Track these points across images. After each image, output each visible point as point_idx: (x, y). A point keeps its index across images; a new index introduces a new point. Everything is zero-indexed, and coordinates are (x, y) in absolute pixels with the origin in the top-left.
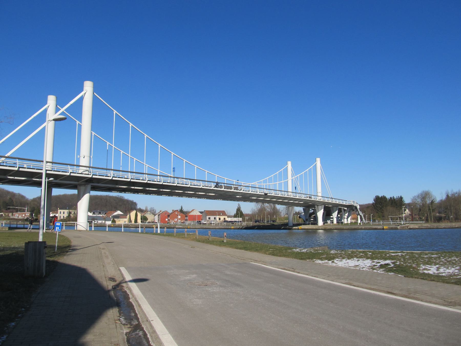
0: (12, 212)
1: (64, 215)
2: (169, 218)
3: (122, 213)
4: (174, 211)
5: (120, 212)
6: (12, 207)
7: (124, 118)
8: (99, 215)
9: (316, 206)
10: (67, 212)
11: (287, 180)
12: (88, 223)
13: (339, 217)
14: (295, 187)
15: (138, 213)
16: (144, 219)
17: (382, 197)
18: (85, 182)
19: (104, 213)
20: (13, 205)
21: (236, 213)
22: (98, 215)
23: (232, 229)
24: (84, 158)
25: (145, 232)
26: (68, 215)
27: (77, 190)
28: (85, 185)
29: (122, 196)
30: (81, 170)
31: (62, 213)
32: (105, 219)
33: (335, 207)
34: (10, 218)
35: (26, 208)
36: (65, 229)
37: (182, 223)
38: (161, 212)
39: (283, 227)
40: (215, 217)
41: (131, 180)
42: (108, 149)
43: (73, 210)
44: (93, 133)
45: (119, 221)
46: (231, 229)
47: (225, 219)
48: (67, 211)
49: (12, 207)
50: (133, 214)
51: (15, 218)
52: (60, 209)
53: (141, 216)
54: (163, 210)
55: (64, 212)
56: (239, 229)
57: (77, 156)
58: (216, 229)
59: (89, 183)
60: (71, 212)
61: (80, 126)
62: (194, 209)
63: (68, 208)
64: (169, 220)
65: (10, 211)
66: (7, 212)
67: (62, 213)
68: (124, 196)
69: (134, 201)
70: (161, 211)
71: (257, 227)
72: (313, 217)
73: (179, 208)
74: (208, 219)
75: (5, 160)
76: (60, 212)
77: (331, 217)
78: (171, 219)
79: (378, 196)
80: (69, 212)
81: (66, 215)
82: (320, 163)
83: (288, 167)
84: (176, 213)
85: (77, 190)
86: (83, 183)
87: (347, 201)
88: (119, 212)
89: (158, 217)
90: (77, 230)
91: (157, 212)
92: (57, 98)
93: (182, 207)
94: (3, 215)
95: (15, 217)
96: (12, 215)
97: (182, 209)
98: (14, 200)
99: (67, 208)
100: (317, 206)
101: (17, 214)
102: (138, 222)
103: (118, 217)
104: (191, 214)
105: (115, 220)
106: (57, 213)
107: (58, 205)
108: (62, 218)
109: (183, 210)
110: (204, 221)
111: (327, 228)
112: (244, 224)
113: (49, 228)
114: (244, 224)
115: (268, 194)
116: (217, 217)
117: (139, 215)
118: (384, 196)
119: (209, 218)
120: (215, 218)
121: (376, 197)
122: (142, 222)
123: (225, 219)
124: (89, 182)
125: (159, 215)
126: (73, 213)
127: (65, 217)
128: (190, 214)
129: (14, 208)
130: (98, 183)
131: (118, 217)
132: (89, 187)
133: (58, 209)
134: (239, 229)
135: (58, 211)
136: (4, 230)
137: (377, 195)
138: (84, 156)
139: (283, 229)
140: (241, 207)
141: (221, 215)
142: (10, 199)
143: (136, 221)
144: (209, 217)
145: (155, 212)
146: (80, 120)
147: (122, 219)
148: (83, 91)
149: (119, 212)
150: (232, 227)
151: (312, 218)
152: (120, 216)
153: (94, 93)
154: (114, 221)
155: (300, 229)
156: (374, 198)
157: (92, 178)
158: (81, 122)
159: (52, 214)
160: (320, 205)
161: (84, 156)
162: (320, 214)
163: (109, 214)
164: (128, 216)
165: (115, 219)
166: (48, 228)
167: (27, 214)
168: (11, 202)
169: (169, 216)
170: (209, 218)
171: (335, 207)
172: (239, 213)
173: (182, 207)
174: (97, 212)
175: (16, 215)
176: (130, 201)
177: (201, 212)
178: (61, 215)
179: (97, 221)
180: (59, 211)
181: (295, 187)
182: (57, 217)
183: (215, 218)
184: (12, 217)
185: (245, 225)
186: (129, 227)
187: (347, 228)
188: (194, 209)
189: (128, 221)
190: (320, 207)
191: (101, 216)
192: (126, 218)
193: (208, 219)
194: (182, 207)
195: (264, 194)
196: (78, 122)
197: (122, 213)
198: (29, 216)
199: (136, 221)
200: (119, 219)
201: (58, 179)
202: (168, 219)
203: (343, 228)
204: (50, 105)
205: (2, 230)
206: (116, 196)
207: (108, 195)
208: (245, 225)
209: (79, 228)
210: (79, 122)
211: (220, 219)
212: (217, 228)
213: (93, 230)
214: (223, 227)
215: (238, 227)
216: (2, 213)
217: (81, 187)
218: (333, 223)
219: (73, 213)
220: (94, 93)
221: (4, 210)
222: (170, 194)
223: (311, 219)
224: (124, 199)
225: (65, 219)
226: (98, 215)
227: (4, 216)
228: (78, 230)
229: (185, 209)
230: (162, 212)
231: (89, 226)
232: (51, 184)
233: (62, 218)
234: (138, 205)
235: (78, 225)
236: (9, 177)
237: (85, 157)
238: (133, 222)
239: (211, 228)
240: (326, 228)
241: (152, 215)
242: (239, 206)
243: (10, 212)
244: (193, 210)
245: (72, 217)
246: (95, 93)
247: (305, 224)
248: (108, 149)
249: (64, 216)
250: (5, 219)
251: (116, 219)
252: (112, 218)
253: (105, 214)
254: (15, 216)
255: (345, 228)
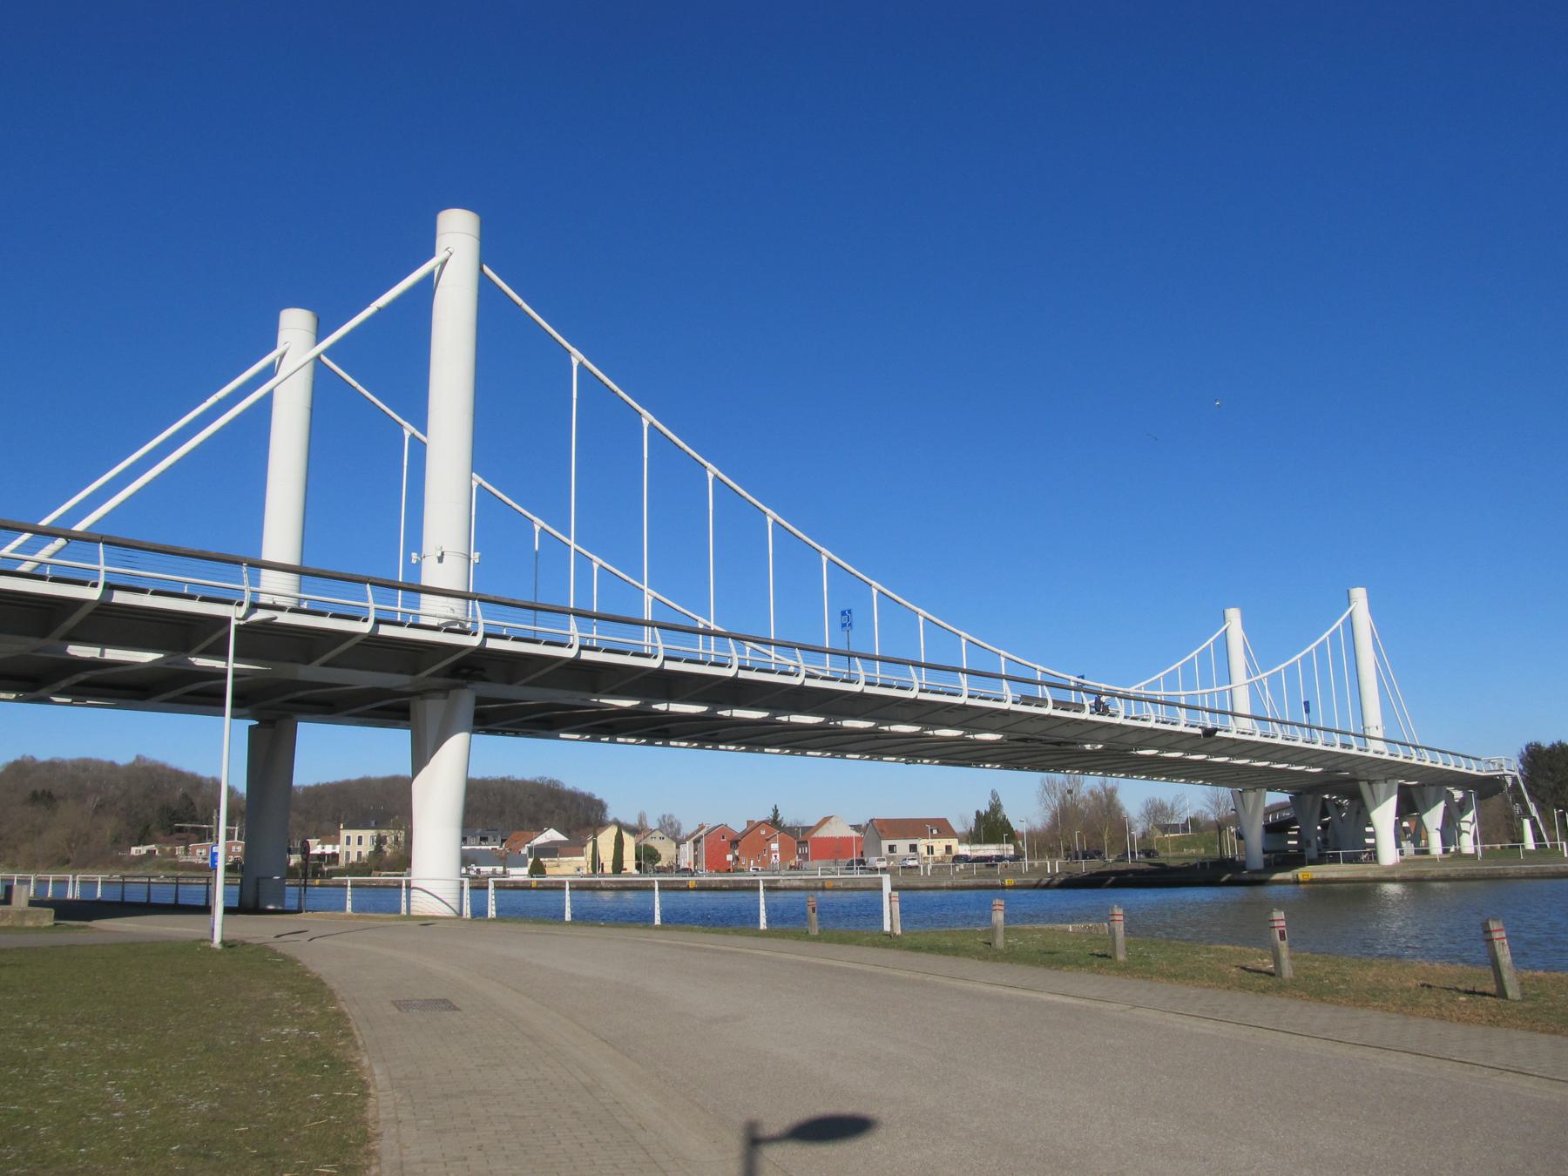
0: (184, 841)
1: (359, 848)
2: (737, 853)
3: (561, 837)
4: (753, 827)
5: (555, 832)
6: (190, 825)
7: (615, 388)
8: (480, 844)
9: (1364, 786)
10: (372, 837)
11: (1229, 687)
12: (462, 882)
13: (1404, 829)
14: (1307, 704)
15: (625, 835)
16: (647, 857)
17: (1553, 746)
18: (446, 676)
19: (499, 838)
20: (193, 819)
21: (973, 826)
22: (478, 847)
23: (1010, 887)
24: (440, 559)
25: (816, 933)
26: (373, 850)
27: (410, 731)
28: (445, 691)
29: (555, 779)
30: (434, 609)
31: (354, 840)
32: (505, 860)
33: (1432, 785)
34: (177, 863)
35: (237, 828)
36: (353, 909)
37: (791, 867)
38: (705, 830)
39: (1229, 875)
40: (913, 842)
41: (663, 663)
42: (537, 548)
43: (393, 831)
44: (477, 479)
45: (558, 866)
46: (1003, 887)
47: (948, 848)
48: (372, 833)
49: (190, 825)
50: (606, 840)
51: (193, 863)
52: (346, 827)
53: (638, 847)
54: (711, 822)
55: (360, 839)
56: (1036, 887)
57: (407, 558)
58: (942, 888)
59: (465, 681)
60: (386, 837)
61: (419, 449)
62: (832, 817)
63: (373, 823)
64: (737, 859)
65: (177, 839)
66: (167, 843)
67: (354, 840)
68: (561, 780)
69: (598, 797)
70: (702, 827)
71: (1113, 878)
72: (1296, 833)
73: (767, 814)
74: (885, 850)
75: (51, 557)
76: (348, 838)
77: (1368, 829)
78: (743, 856)
79: (1538, 746)
80: (379, 835)
81: (367, 848)
82: (1370, 611)
83: (1228, 630)
84: (763, 833)
85: (410, 731)
86: (440, 681)
87: (1479, 760)
88: (552, 835)
89: (695, 850)
90: (409, 917)
91: (687, 829)
92: (318, 320)
93: (776, 811)
94: (157, 852)
95: (195, 860)
96: (186, 850)
97: (779, 819)
98: (197, 800)
99: (370, 824)
100: (1370, 783)
101: (201, 848)
102: (626, 869)
103: (551, 850)
104: (823, 833)
105: (541, 863)
106: (336, 842)
107: (342, 817)
108: (353, 858)
109: (781, 821)
110: (878, 860)
111: (1429, 875)
112: (1053, 868)
113: (283, 906)
114: (1053, 868)
115: (1218, 734)
116: (922, 845)
117: (630, 843)
118: (1560, 743)
119: (891, 848)
120: (913, 848)
121: (1527, 748)
122: (638, 867)
123: (948, 848)
124: (465, 677)
125: (697, 842)
126: (390, 840)
127: (364, 854)
128: (815, 835)
129: (197, 829)
130: (510, 682)
131: (551, 850)
132: (466, 701)
133: (342, 827)
134: (1036, 887)
135: (339, 835)
136: (30, 924)
137: (1533, 739)
138: (443, 554)
139: (1229, 883)
140: (1002, 803)
141: (934, 837)
142: (185, 796)
143: (618, 866)
144: (892, 842)
145: (678, 830)
146: (419, 413)
147: (567, 859)
148: (434, 256)
149: (552, 835)
150: (1008, 882)
151: (1293, 838)
152: (559, 846)
153: (481, 269)
154: (538, 869)
155: (1304, 882)
156: (1522, 753)
157: (481, 651)
158: (424, 431)
159: (320, 846)
160: (1382, 777)
161: (439, 555)
162: (1384, 816)
163: (516, 841)
164: (590, 846)
165: (541, 859)
166: (280, 908)
167: (234, 848)
168: (187, 809)
169: (735, 843)
170: (891, 848)
171: (1433, 789)
172: (991, 826)
173: (776, 811)
174: (474, 836)
175: (198, 851)
176: (582, 795)
177: (856, 828)
178: (349, 848)
179: (475, 868)
180: (344, 834)
181: (1307, 704)
182: (338, 855)
183: (913, 848)
184: (184, 860)
185: (1057, 871)
186: (598, 886)
187: (1523, 872)
188: (832, 817)
189: (590, 865)
190: (1381, 788)
191: (490, 848)
192: (583, 855)
193: (885, 850)
194: (777, 811)
195: (1199, 731)
196: (409, 430)
197: (561, 837)
198: (240, 854)
199: (618, 866)
200: (556, 859)
201: (318, 657)
202: (733, 853)
203: (1502, 872)
204: (288, 349)
205: (17, 924)
206: (535, 781)
207: (509, 777)
208: (1057, 871)
209: (423, 904)
210: (413, 429)
211: (930, 850)
212: (944, 884)
213: (312, 842)
214: (971, 882)
215: (1034, 880)
216: (153, 847)
217: (428, 702)
218: (1426, 852)
219: (390, 840)
220: (481, 269)
221: (159, 835)
222: (797, 743)
223: (1289, 842)
224: (563, 788)
225: (366, 861)
226: (478, 847)
227: (157, 857)
228: (413, 913)
229: (787, 818)
230: (709, 832)
231: (470, 888)
232: (289, 697)
233: (353, 858)
234: (608, 811)
235: (414, 893)
236: (77, 651)
237: (445, 557)
238: (608, 868)
239: (921, 885)
240: (1422, 875)
241: (670, 840)
242: (994, 798)
243: (180, 841)
244: (826, 820)
245: (388, 854)
246: (486, 268)
247: (1320, 860)
248: (537, 548)
249: (359, 853)
250: (160, 866)
251: (547, 859)
252: (530, 856)
253: (503, 841)
254: (194, 854)
255: (1512, 871)
